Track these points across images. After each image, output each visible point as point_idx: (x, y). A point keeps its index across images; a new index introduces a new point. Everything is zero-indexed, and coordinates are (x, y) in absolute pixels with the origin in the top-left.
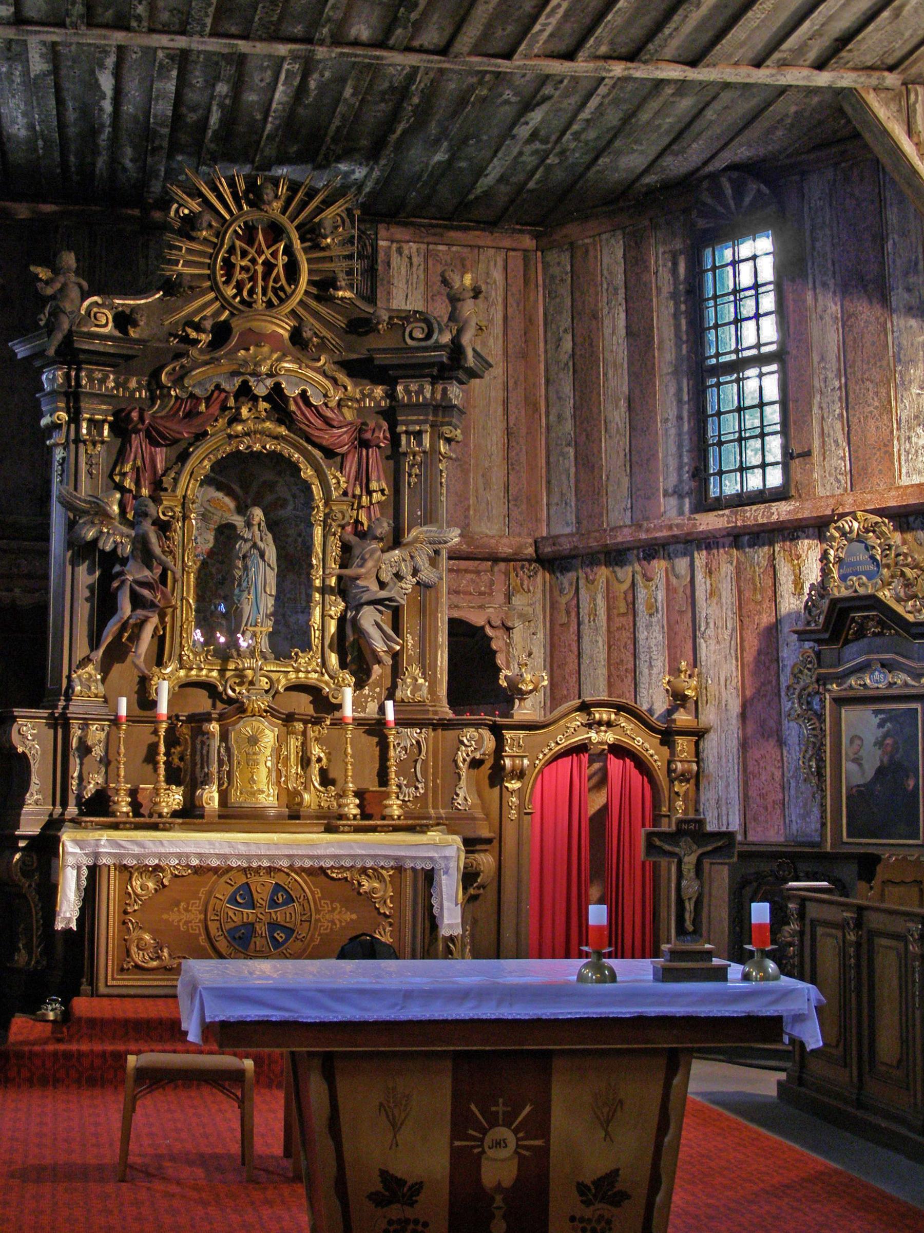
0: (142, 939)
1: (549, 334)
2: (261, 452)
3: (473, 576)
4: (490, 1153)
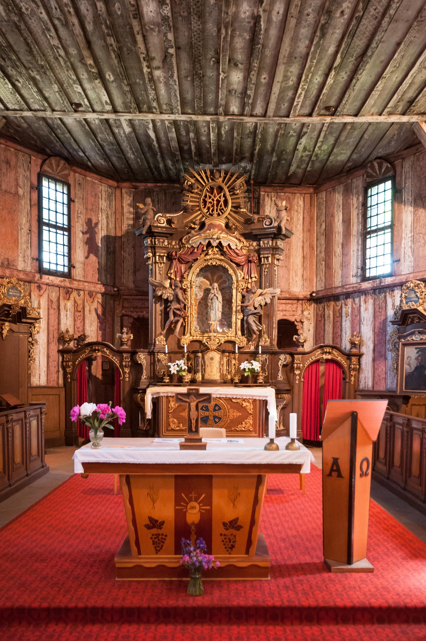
3: (291, 305)
4: (190, 511)
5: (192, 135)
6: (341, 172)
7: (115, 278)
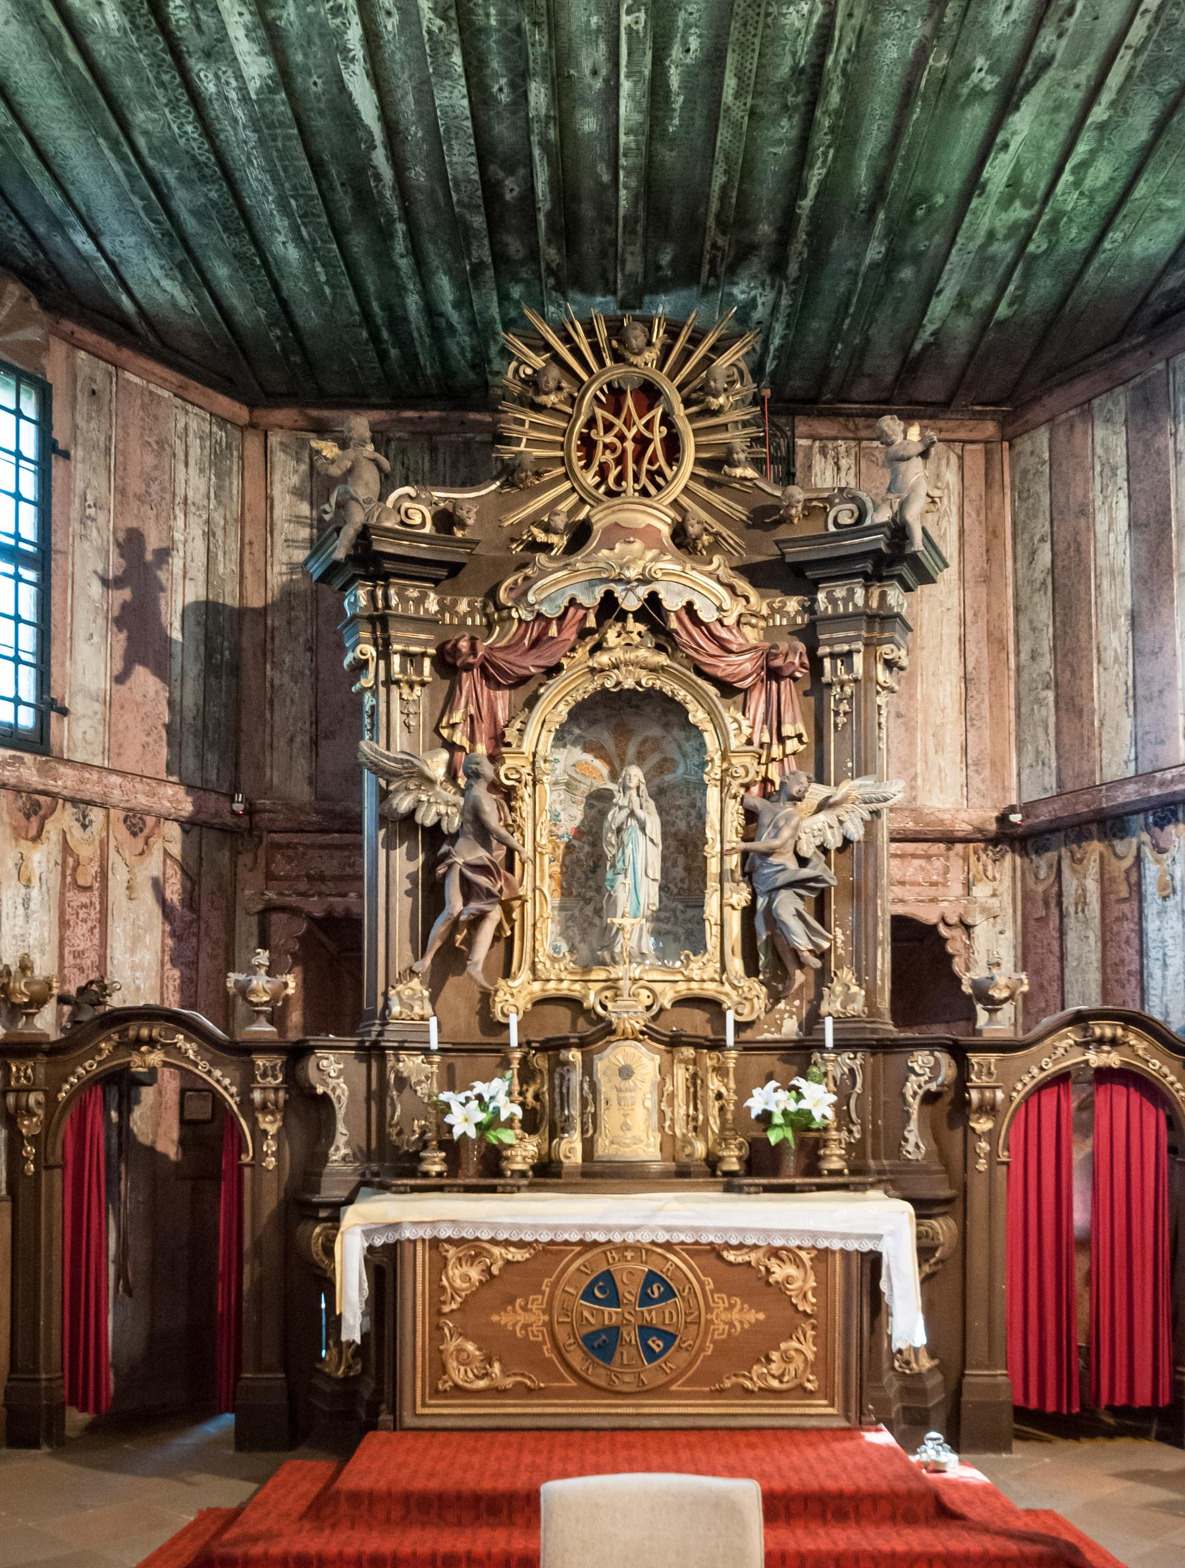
0: (464, 1350)
1: (1019, 548)
2: (635, 690)
3: (922, 862)
5: (538, 95)
6: (1127, 329)
7: (237, 765)
